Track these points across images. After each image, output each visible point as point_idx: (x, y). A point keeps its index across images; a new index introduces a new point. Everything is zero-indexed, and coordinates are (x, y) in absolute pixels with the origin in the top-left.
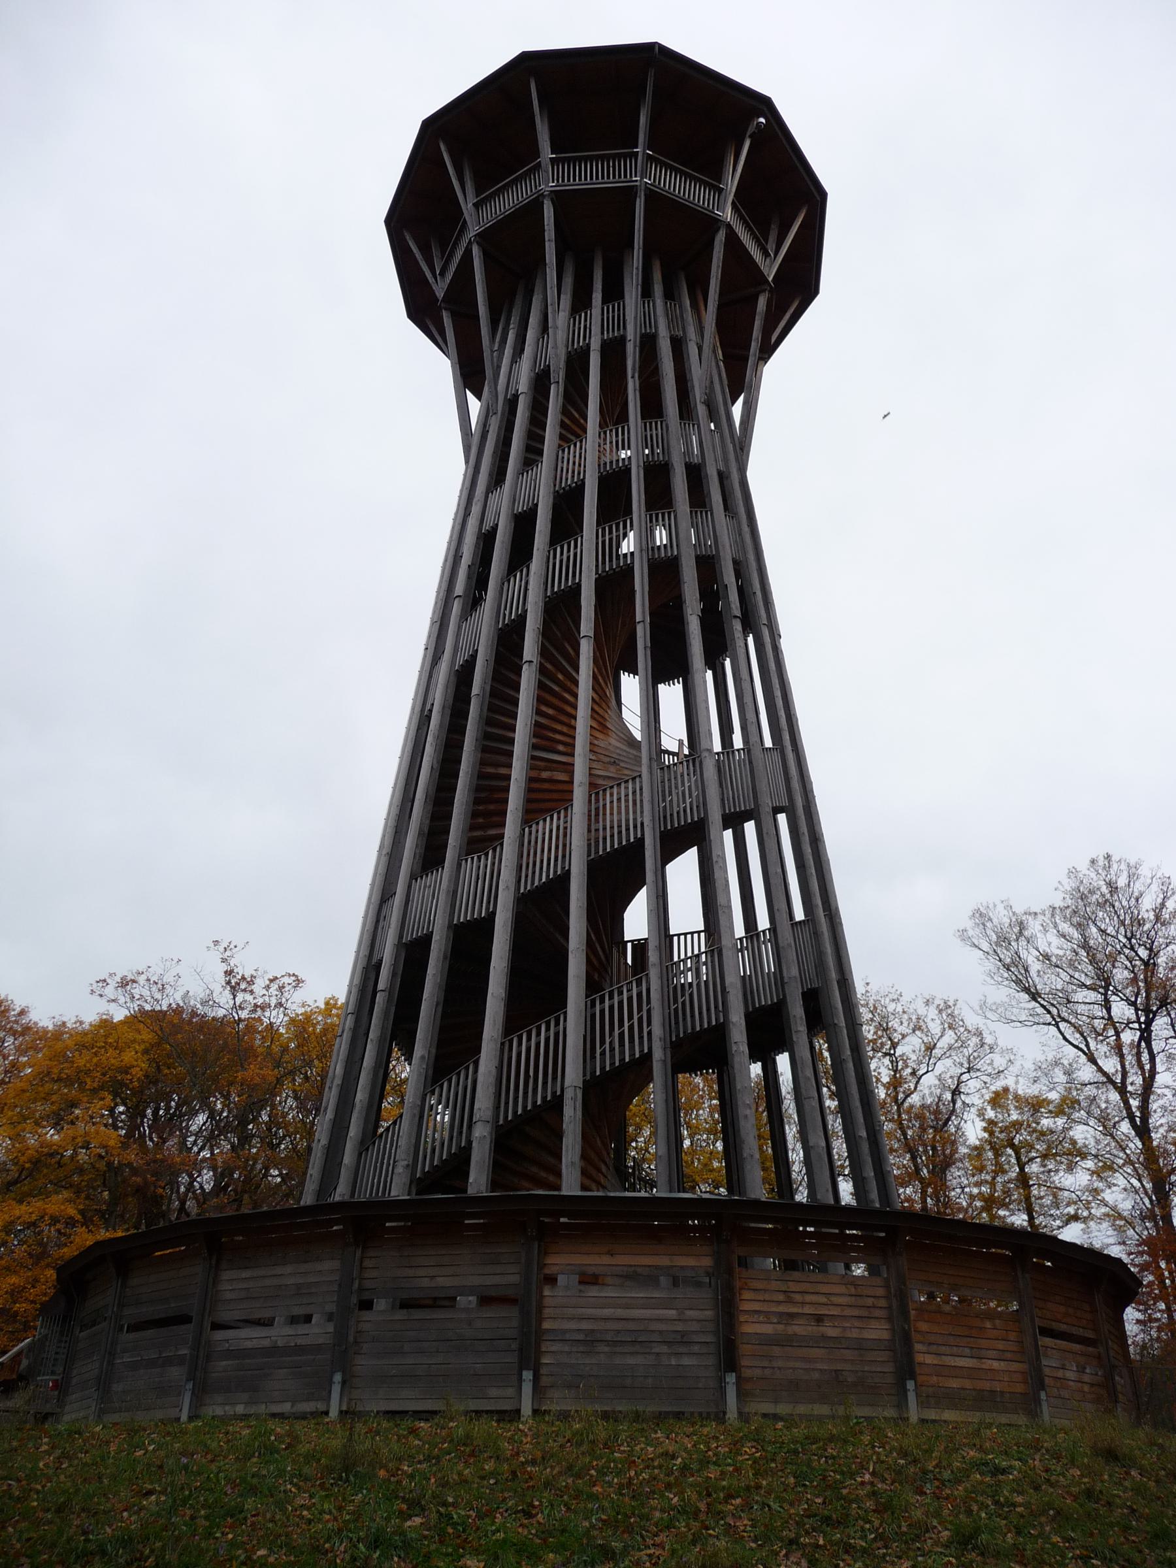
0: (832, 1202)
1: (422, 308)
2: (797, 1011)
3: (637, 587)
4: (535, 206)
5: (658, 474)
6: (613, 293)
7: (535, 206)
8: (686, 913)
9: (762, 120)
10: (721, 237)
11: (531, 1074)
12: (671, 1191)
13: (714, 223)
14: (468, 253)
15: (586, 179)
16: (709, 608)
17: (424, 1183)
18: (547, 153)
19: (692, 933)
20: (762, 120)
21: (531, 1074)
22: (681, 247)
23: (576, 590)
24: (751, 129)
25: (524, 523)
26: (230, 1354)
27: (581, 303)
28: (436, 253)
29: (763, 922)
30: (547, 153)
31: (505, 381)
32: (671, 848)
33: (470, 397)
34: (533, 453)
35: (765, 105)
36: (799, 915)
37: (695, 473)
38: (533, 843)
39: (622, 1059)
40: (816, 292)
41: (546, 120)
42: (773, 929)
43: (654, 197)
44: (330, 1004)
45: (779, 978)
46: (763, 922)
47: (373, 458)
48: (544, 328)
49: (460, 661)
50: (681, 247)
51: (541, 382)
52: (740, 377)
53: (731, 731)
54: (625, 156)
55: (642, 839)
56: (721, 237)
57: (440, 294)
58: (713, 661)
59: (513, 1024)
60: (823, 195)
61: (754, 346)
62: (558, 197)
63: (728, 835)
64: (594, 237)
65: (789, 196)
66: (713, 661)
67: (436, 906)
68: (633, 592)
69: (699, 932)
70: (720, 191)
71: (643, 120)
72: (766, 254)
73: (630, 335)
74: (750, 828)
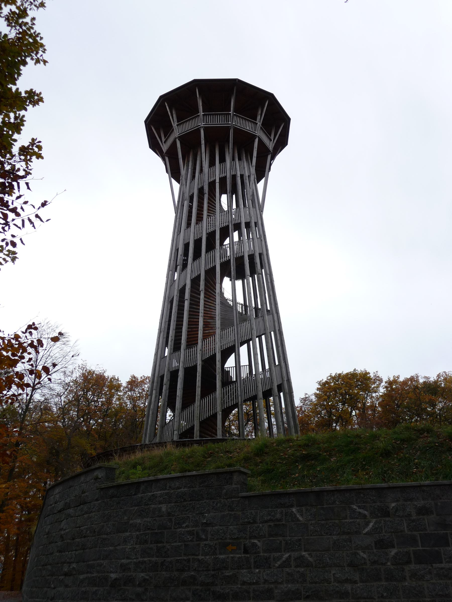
4: (198, 131)
6: (223, 160)
8: (244, 361)
10: (257, 140)
13: (254, 137)
16: (252, 265)
17: (182, 435)
22: (244, 143)
23: (214, 267)
25: (198, 242)
27: (212, 164)
29: (267, 367)
32: (242, 344)
34: (199, 219)
36: (277, 363)
40: (287, 144)
42: (270, 368)
43: (237, 131)
44: (134, 383)
45: (271, 378)
46: (267, 367)
48: (201, 170)
49: (180, 287)
50: (244, 143)
51: (201, 190)
53: (257, 298)
54: (227, 114)
55: (235, 345)
56: (257, 140)
58: (252, 275)
59: (203, 396)
60: (289, 119)
62: (206, 129)
63: (257, 339)
64: (217, 139)
66: (252, 275)
67: (179, 363)
73: (228, 176)
74: (263, 337)
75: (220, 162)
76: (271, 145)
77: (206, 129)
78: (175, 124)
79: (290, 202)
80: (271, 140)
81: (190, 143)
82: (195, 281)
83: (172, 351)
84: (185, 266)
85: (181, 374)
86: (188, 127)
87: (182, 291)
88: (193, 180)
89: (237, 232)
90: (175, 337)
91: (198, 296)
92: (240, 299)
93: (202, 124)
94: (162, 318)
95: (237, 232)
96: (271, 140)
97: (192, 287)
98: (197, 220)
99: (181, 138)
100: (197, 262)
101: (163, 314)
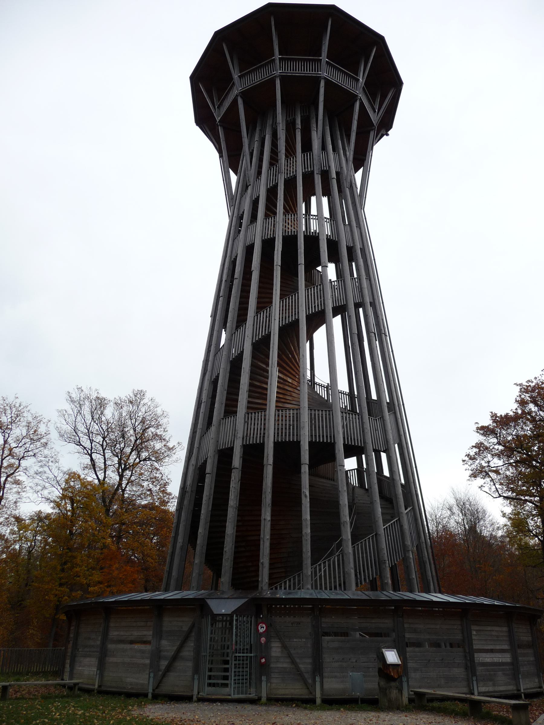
1: (204, 119)
4: (272, 82)
5: (308, 178)
13: (354, 97)
14: (235, 101)
18: (277, 56)
19: (352, 470)
22: (340, 107)
26: (483, 664)
30: (277, 56)
31: (394, 426)
33: (232, 173)
34: (265, 302)
35: (379, 41)
37: (325, 175)
38: (280, 434)
43: (328, 83)
47: (178, 206)
52: (361, 159)
62: (283, 79)
65: (386, 83)
69: (354, 470)
75: (303, 151)
76: (375, 118)
77: (283, 79)
78: (236, 76)
79: (407, 197)
80: (375, 111)
81: (259, 104)
82: (261, 346)
83: (222, 416)
84: (241, 319)
85: (237, 461)
86: (257, 78)
87: (235, 365)
88: (238, 327)
89: (339, 317)
90: (240, 304)
91: (265, 374)
92: (343, 385)
93: (278, 72)
94: (239, 183)
95: (339, 317)
96: (375, 111)
97: (254, 356)
98: (258, 308)
99: (244, 94)
100: (263, 315)
101: (230, 233)
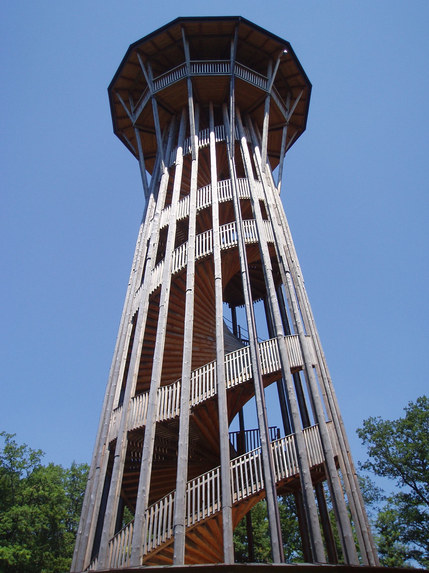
0: (368, 564)
1: (121, 129)
2: (333, 466)
3: (242, 255)
7: (184, 81)
9: (285, 51)
10: (268, 100)
11: (204, 500)
12: (281, 562)
13: (265, 94)
15: (207, 71)
18: (188, 60)
20: (285, 51)
21: (204, 500)
24: (281, 55)
25: (182, 225)
28: (131, 102)
30: (188, 60)
39: (285, 476)
41: (188, 44)
57: (134, 121)
61: (282, 150)
65: (295, 85)
68: (239, 259)
70: (267, 80)
71: (233, 49)
72: (286, 110)
